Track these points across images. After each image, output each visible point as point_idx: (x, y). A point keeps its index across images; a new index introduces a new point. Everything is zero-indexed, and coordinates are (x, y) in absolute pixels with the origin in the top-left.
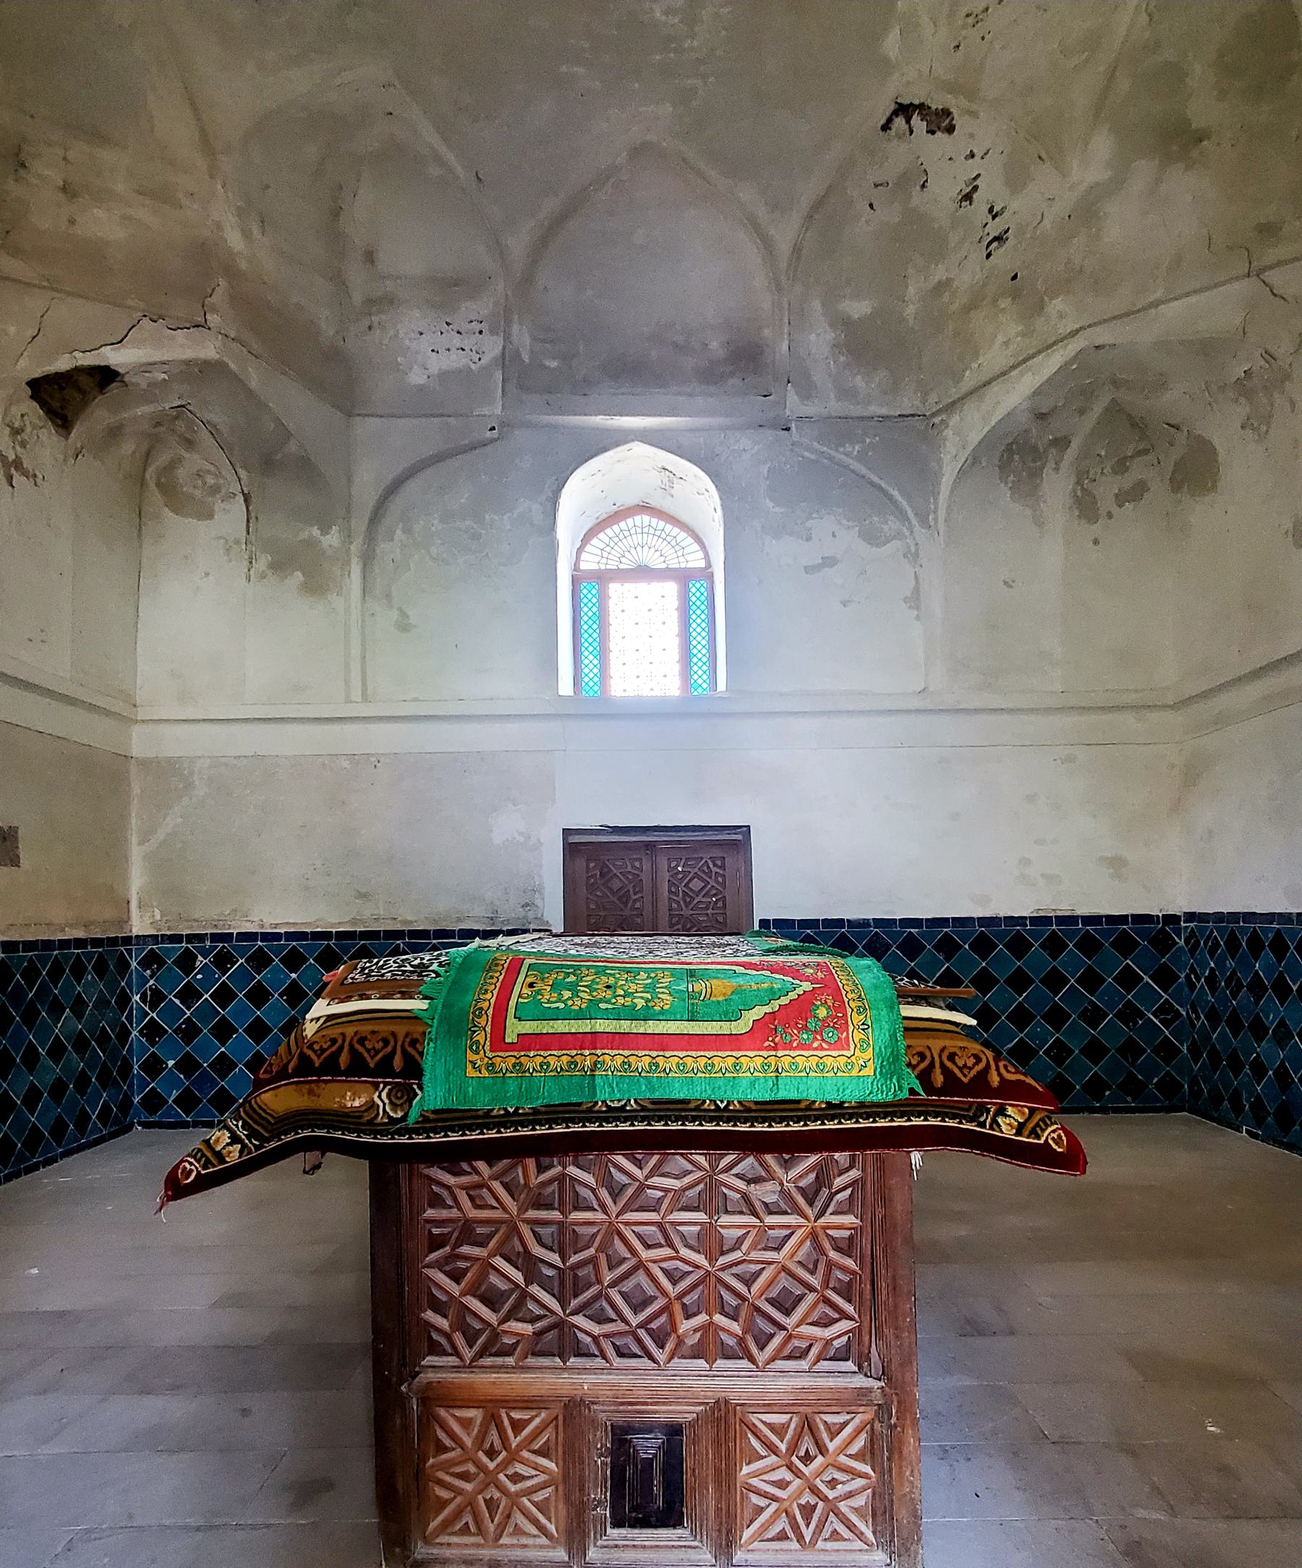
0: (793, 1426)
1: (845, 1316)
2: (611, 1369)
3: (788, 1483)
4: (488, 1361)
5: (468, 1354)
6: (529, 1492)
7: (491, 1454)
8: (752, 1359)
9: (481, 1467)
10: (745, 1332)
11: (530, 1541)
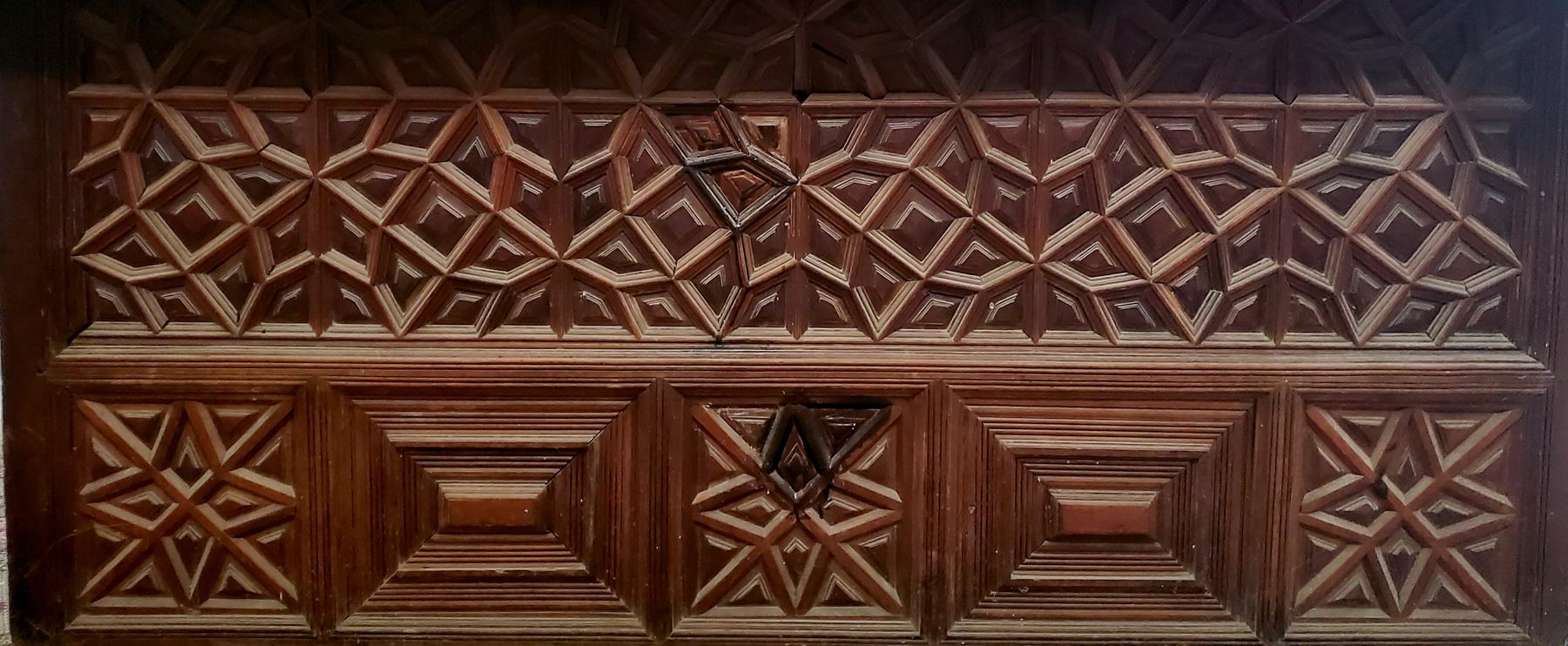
0: (167, 418)
1: (1495, 257)
2: (156, 339)
3: (770, 516)
4: (742, 333)
5: (715, 321)
6: (249, 531)
7: (190, 475)
8: (862, 324)
9: (171, 494)
10: (377, 280)
11: (1461, 614)
